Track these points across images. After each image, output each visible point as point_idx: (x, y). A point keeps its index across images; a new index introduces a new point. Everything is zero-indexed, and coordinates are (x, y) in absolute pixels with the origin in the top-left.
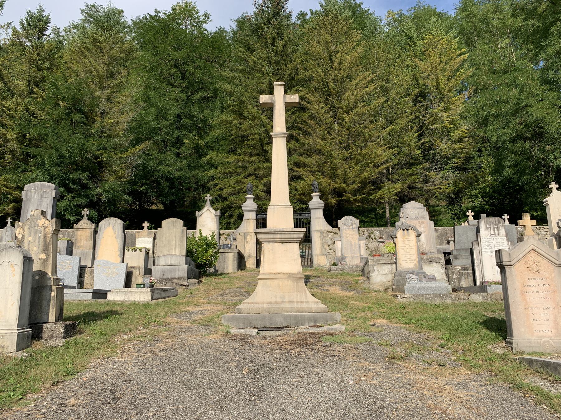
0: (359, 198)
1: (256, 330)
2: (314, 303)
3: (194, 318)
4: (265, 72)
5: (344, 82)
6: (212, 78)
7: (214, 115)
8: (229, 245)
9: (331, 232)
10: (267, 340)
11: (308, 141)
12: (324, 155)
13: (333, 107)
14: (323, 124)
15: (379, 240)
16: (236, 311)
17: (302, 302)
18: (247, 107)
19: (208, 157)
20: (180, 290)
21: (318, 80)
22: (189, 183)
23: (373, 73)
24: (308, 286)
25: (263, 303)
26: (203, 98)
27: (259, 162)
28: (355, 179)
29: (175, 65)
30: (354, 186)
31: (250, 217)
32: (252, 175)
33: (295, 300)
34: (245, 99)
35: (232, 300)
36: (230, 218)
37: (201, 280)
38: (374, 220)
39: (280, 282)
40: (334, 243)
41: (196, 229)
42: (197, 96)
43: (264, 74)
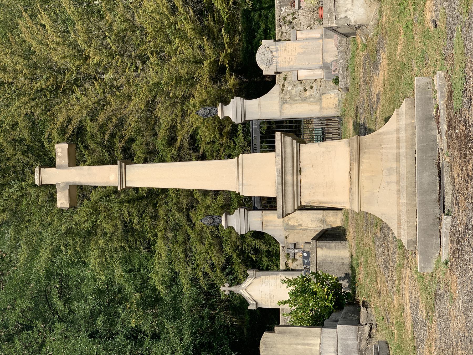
0: (226, 39)
1: (444, 217)
2: (398, 120)
3: (424, 318)
4: (19, 194)
5: (35, 63)
6: (29, 282)
7: (90, 277)
8: (305, 254)
9: (283, 86)
10: (460, 200)
11: (132, 122)
12: (155, 97)
13: (76, 82)
14: (105, 99)
15: (296, 7)
16: (412, 248)
17: (398, 140)
18: (76, 224)
19: (160, 287)
20: (378, 337)
21: (32, 107)
22: (202, 318)
23: (21, 16)
24: (372, 127)
25: (399, 204)
26: (62, 295)
27: (166, 203)
28: (195, 45)
29: (8, 340)
30: (206, 48)
31: (257, 220)
32: (188, 216)
33: (395, 151)
34: (64, 227)
35: (394, 253)
36: (260, 253)
37: (361, 303)
38: (264, 12)
39: (364, 175)
40: (301, 81)
41: (279, 309)
42: (60, 305)
43: (23, 196)
